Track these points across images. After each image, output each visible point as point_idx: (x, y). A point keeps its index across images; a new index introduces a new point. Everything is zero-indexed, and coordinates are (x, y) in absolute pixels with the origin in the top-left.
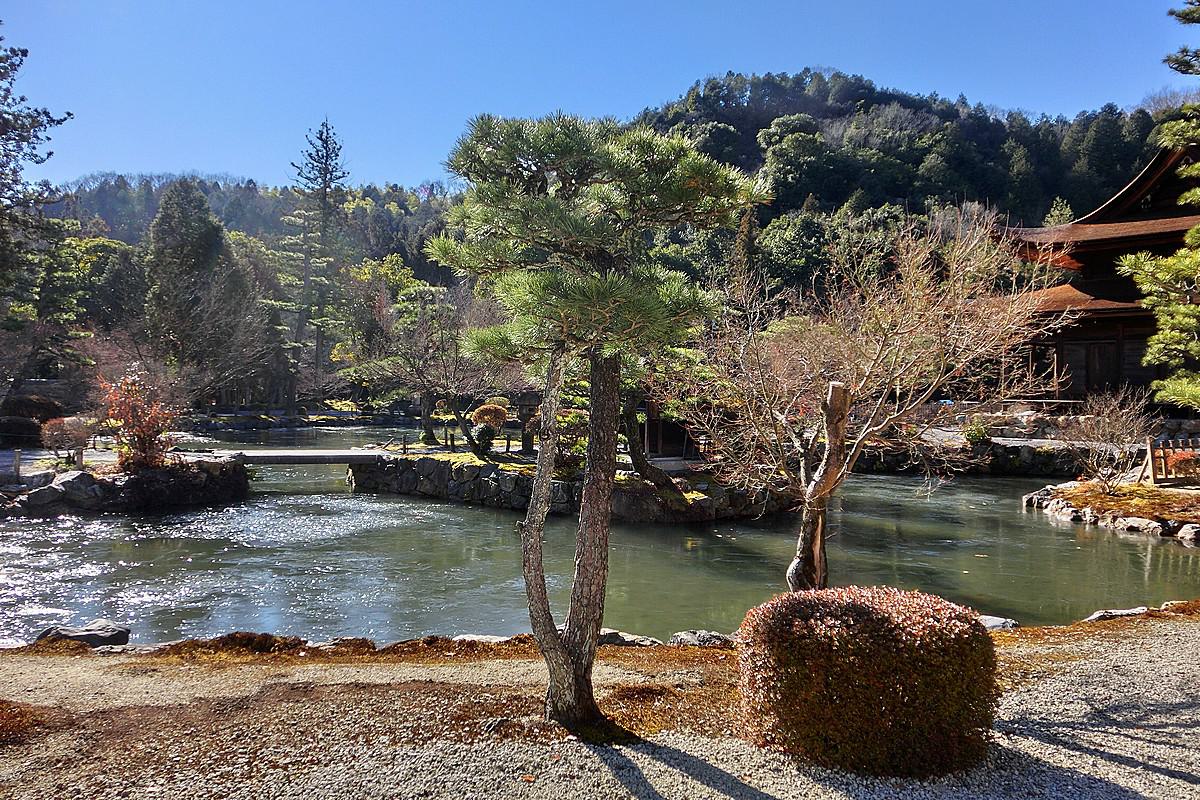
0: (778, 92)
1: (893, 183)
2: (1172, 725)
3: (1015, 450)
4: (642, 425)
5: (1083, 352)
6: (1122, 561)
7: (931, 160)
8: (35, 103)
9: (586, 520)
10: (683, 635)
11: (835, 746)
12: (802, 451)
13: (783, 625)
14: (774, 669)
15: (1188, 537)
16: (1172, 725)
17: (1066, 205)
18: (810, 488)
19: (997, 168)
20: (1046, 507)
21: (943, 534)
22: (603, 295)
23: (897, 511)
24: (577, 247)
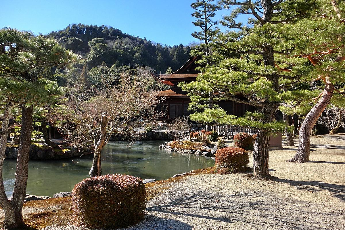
0: (94, 32)
1: (125, 59)
2: (190, 202)
3: (158, 133)
4: (48, 129)
5: (174, 107)
6: (183, 161)
7: (137, 54)
9: (20, 161)
10: (58, 194)
11: (101, 223)
12: (94, 136)
13: (85, 188)
14: (82, 202)
15: (197, 154)
16: (190, 202)
18: (96, 147)
19: (152, 56)
20: (165, 148)
21: (140, 157)
22: (23, 88)
23: (127, 151)
24: (16, 72)
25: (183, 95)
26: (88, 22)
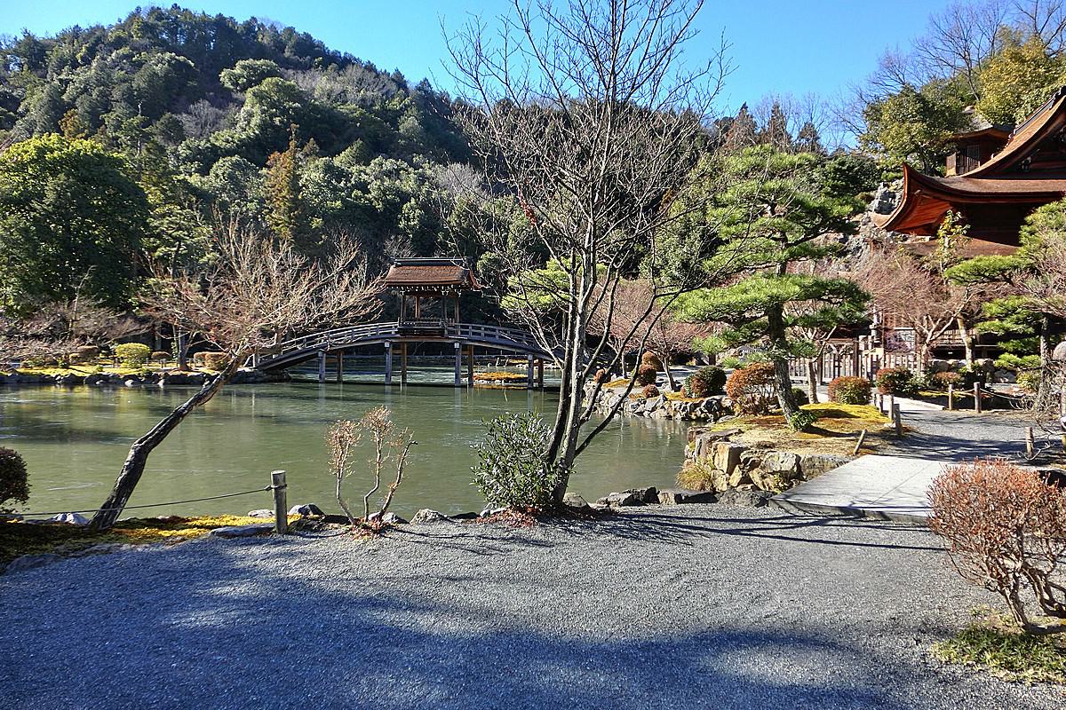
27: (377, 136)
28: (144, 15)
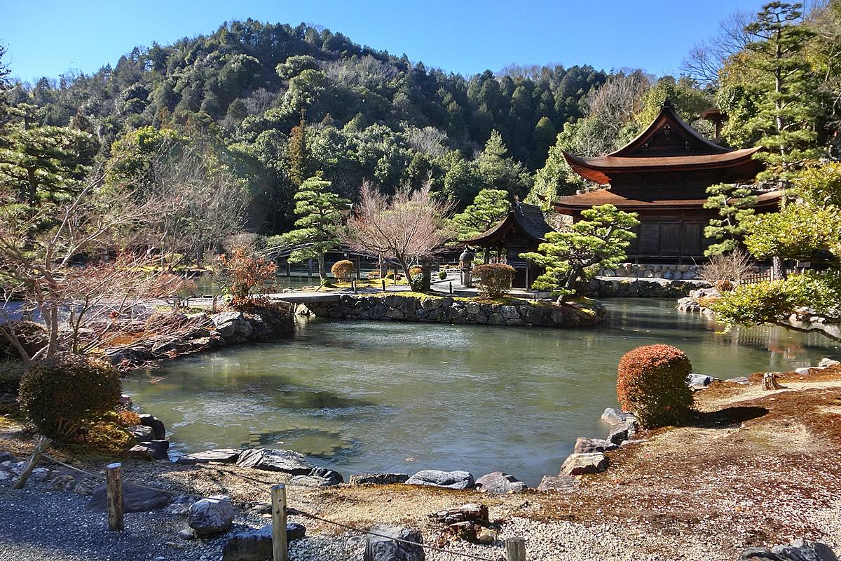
0: (285, 41)
7: (400, 97)
8: (402, 55)
17: (499, 134)
25: (644, 203)
26: (269, 17)
27: (376, 109)
28: (229, 28)
